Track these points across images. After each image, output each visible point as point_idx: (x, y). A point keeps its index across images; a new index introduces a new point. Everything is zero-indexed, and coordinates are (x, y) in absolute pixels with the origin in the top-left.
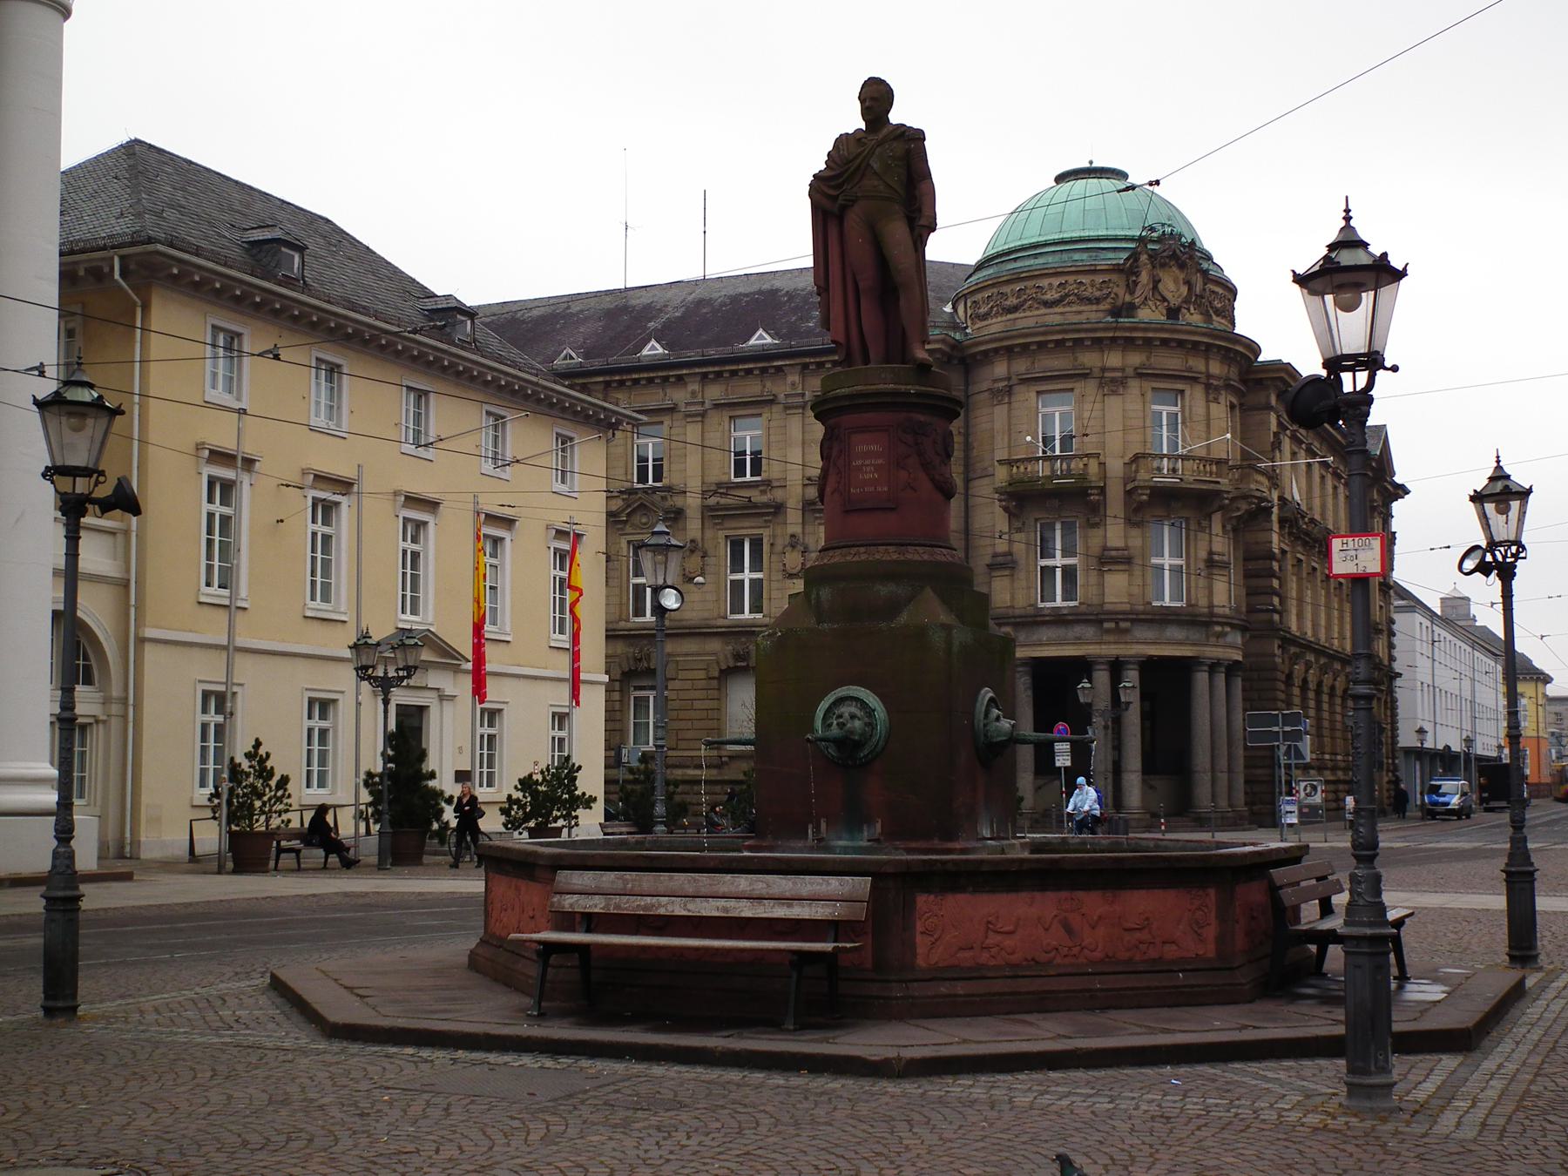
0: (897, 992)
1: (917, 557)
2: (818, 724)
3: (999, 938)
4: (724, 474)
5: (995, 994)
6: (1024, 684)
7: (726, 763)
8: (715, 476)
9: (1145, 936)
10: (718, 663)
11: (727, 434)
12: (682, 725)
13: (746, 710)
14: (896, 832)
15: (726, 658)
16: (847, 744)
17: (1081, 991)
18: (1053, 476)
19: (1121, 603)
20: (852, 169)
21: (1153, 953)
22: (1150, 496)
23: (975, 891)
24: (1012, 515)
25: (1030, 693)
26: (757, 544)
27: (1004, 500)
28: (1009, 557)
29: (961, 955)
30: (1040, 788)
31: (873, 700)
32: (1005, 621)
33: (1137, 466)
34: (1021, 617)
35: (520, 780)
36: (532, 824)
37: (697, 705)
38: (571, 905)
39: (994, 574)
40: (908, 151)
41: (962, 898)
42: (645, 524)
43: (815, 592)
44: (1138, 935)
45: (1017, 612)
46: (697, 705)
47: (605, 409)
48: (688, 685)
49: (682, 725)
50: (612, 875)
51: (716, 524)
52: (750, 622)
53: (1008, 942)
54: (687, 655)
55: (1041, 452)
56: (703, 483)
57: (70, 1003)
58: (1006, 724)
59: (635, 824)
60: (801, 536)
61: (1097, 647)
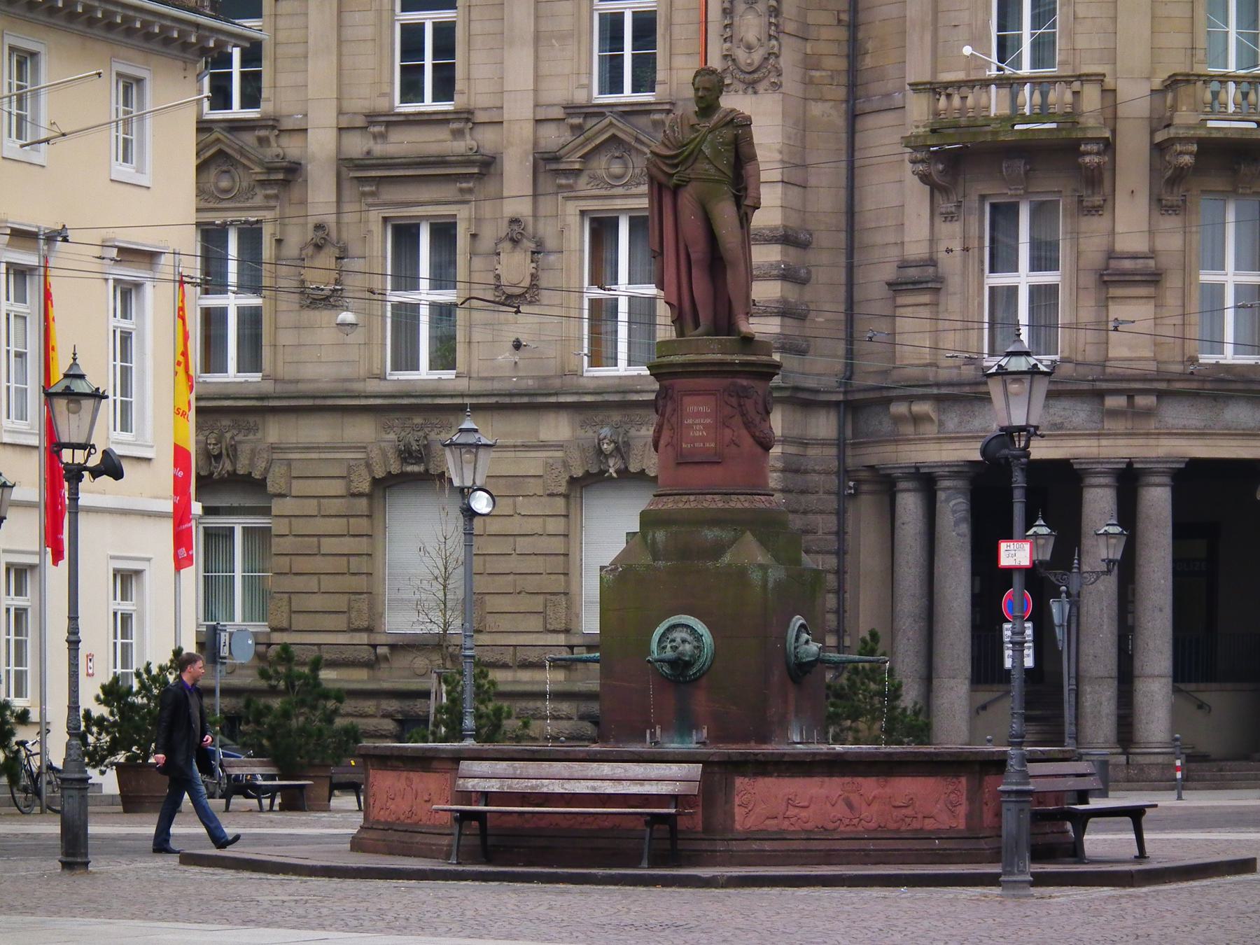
0: (720, 846)
1: (739, 506)
2: (654, 646)
3: (797, 810)
4: (383, 95)
5: (793, 851)
6: (954, 512)
7: (386, 659)
8: (363, 99)
9: (909, 811)
10: (368, 466)
11: (386, 15)
12: (299, 583)
13: (426, 560)
14: (718, 736)
15: (384, 454)
16: (681, 665)
17: (858, 850)
18: (1015, 116)
19: (1140, 359)
20: (686, 153)
21: (916, 825)
22: (1197, 155)
23: (779, 776)
24: (936, 188)
25: (965, 528)
26: (444, 233)
27: (922, 161)
28: (931, 270)
29: (768, 822)
30: (984, 707)
31: (701, 627)
32: (920, 391)
33: (1175, 99)
34: (950, 384)
35: (103, 687)
36: (121, 757)
37: (328, 545)
38: (473, 786)
39: (901, 300)
40: (736, 137)
41: (768, 780)
42: (226, 191)
43: (651, 534)
44: (904, 811)
45: (944, 375)
46: (328, 545)
47: (198, 26)
48: (311, 507)
49: (299, 583)
50: (504, 764)
51: (364, 194)
52: (430, 387)
53: (804, 814)
54: (308, 449)
55: (994, 68)
56: (340, 112)
57: (84, 860)
58: (814, 647)
59: (275, 762)
60: (530, 220)
61: (1094, 442)
